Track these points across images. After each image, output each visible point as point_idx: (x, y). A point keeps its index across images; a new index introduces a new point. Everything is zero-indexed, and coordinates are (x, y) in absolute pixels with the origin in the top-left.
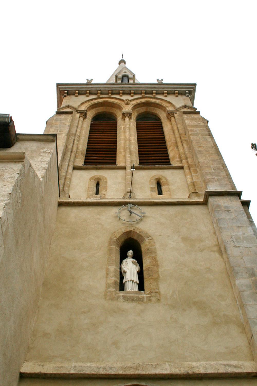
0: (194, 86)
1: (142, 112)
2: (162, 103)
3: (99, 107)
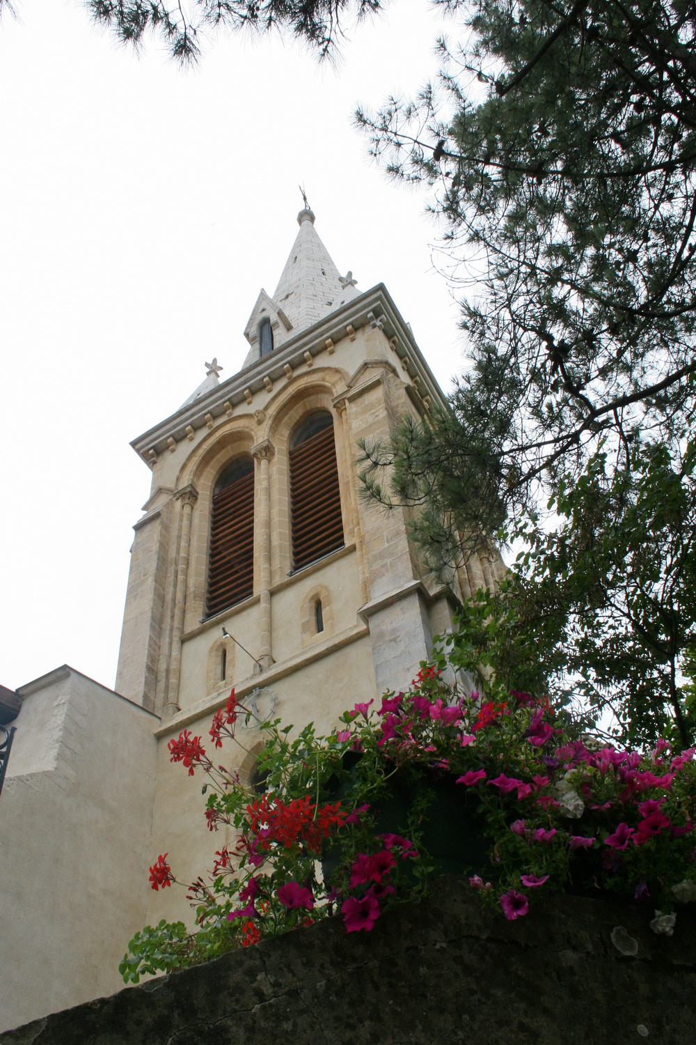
0: (380, 293)
1: (298, 418)
2: (324, 380)
3: (220, 451)
